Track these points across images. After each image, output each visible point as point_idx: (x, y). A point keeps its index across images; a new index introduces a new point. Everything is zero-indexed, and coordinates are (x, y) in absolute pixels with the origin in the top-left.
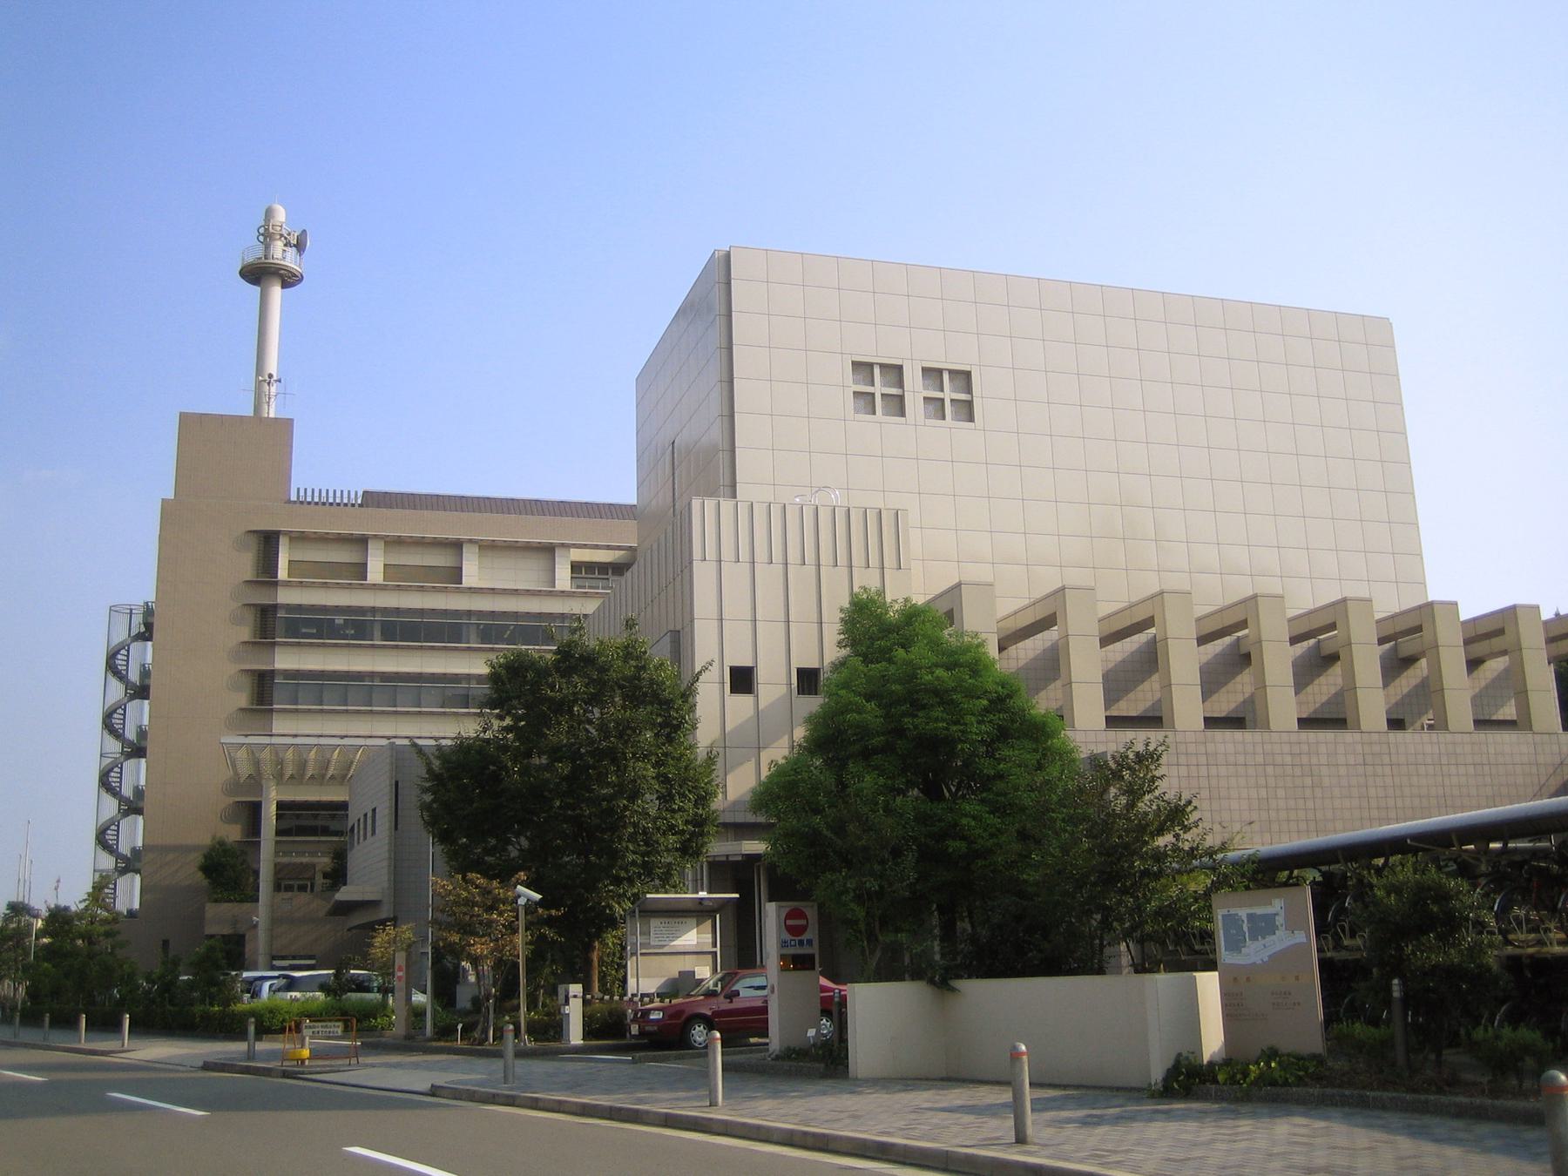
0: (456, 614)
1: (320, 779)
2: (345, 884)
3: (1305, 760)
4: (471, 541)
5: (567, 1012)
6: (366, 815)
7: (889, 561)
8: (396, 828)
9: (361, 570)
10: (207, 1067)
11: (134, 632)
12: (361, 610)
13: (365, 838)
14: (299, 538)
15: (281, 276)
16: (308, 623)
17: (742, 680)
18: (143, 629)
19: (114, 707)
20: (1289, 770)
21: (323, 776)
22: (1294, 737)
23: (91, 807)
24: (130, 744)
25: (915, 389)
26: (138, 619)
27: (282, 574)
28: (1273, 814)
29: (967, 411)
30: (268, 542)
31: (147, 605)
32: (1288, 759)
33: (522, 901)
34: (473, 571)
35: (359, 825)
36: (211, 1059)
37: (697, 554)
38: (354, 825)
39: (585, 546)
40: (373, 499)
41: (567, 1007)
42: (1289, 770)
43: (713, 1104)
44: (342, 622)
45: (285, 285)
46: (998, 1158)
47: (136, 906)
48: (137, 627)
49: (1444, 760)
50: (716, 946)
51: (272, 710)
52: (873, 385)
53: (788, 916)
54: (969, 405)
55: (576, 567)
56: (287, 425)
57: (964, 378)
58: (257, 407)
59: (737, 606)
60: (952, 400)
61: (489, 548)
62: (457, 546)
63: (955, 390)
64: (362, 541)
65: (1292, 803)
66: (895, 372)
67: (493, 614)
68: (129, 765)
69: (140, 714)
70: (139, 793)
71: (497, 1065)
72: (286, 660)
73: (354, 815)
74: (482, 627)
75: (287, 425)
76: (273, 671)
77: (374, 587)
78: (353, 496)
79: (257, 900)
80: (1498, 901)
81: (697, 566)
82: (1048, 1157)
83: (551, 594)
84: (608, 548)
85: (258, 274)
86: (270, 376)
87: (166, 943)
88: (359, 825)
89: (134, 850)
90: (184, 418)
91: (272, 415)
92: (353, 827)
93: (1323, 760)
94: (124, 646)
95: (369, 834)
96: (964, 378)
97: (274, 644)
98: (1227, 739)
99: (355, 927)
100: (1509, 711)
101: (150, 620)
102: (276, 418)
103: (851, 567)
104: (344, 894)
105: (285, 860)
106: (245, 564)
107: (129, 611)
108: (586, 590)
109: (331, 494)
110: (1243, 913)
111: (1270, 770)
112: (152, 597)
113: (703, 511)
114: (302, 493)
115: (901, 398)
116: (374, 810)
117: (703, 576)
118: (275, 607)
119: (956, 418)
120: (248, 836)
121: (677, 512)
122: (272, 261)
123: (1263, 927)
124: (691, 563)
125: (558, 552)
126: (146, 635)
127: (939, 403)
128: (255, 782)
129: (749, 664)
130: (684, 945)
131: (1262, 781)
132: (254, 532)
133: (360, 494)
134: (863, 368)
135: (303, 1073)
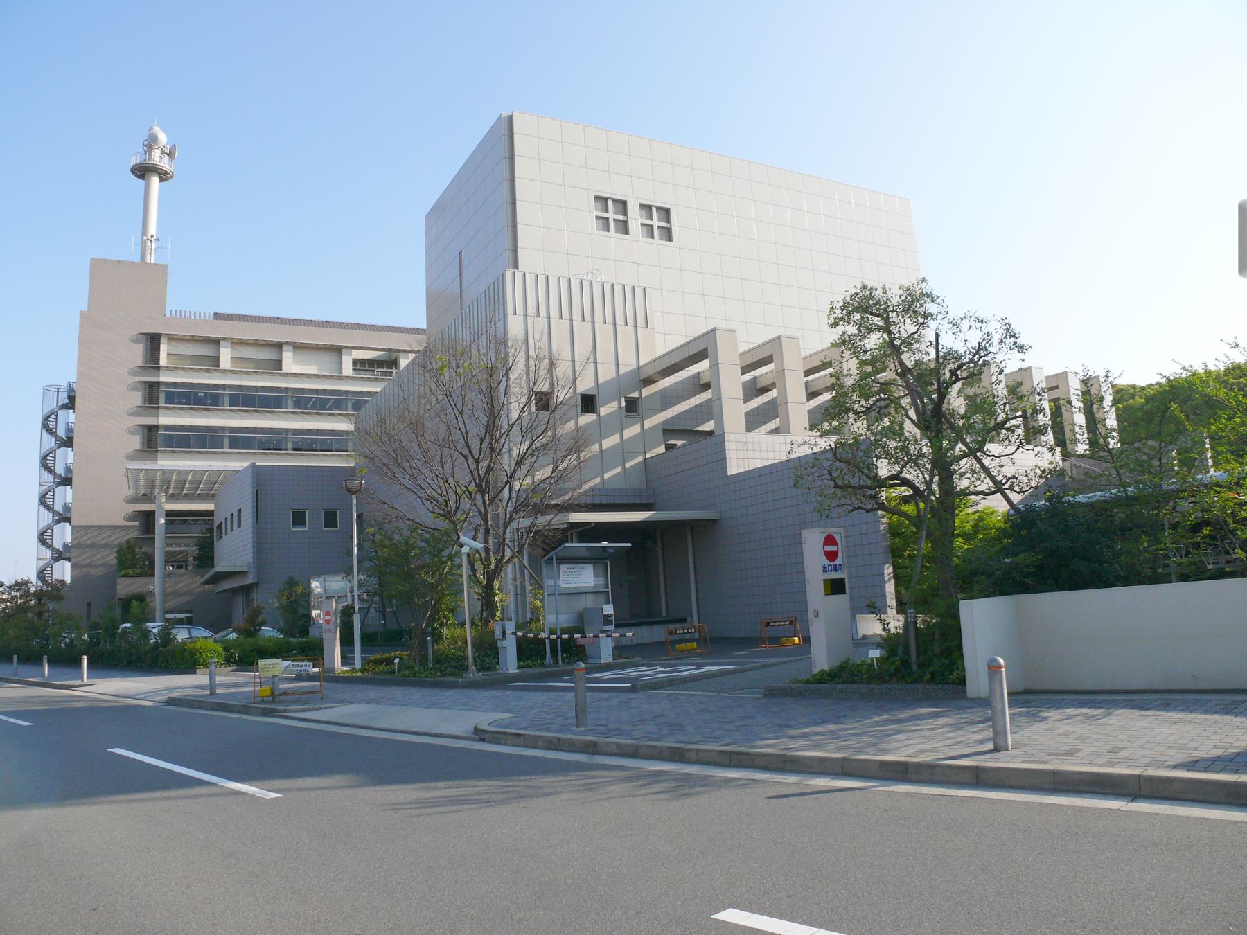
0: (279, 389)
4: (287, 343)
5: (505, 646)
6: (232, 515)
7: (640, 322)
9: (216, 361)
10: (171, 702)
11: (60, 404)
12: (216, 386)
13: (232, 530)
14: (172, 338)
15: (159, 173)
19: (47, 453)
21: (194, 494)
23: (37, 518)
24: (58, 551)
25: (635, 218)
27: (163, 361)
29: (667, 234)
30: (153, 341)
31: (70, 385)
33: (465, 550)
34: (290, 362)
35: (226, 523)
36: (174, 695)
38: (221, 523)
39: (361, 348)
41: (504, 641)
44: (203, 395)
45: (161, 180)
46: (1092, 773)
48: (63, 398)
50: (608, 587)
54: (669, 230)
55: (355, 362)
56: (163, 268)
57: (665, 213)
60: (659, 227)
61: (298, 347)
62: (279, 346)
64: (216, 342)
66: (622, 205)
67: (302, 390)
68: (59, 490)
69: (66, 457)
70: (67, 508)
72: (166, 419)
74: (294, 399)
75: (163, 268)
77: (224, 371)
79: (153, 575)
80: (608, 563)
81: (510, 318)
82: (1100, 766)
83: (340, 378)
84: (376, 349)
85: (142, 171)
87: (89, 604)
88: (226, 523)
89: (65, 545)
90: (95, 262)
91: (153, 262)
94: (54, 412)
95: (229, 531)
99: (224, 591)
101: (72, 394)
106: (138, 353)
107: (56, 390)
108: (362, 376)
112: (73, 378)
116: (239, 511)
118: (156, 427)
120: (143, 534)
121: (466, 306)
122: (153, 162)
125: (344, 351)
128: (148, 497)
130: (585, 587)
132: (145, 334)
133: (212, 315)
134: (602, 200)
135: (285, 711)
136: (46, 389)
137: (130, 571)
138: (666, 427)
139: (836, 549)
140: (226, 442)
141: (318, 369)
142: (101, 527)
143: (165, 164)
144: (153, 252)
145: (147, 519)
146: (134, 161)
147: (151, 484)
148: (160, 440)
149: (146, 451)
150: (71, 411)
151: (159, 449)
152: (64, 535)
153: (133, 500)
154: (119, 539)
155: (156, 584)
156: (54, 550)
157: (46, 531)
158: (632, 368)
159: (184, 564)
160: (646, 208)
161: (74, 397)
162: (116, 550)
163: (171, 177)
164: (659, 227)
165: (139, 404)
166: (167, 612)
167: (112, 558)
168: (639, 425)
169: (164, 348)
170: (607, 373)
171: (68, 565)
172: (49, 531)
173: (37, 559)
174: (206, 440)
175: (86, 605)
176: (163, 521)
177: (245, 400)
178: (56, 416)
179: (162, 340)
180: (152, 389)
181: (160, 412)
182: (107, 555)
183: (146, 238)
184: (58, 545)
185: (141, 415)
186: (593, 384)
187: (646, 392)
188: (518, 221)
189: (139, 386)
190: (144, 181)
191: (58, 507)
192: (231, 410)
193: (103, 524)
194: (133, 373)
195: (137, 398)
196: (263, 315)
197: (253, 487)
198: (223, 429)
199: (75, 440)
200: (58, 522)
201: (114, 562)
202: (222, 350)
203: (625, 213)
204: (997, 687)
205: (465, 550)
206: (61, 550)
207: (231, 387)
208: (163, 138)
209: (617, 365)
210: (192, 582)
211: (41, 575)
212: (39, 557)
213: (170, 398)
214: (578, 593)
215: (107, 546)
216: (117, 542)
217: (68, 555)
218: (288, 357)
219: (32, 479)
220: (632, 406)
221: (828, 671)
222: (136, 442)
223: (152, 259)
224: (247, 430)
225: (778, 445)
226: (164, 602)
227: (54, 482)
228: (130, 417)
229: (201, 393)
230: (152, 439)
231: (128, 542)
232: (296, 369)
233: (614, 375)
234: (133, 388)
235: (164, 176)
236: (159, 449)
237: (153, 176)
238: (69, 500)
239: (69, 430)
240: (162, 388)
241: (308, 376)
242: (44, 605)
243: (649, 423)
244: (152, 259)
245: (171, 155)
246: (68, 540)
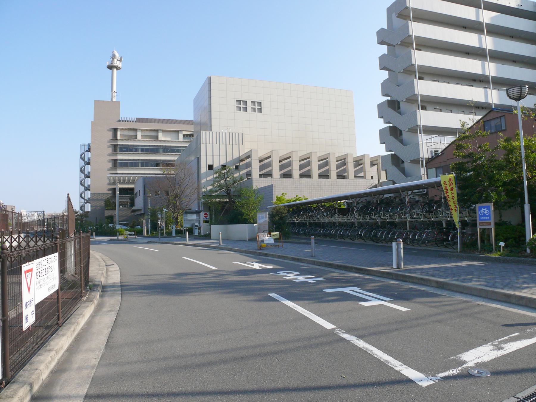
1: (128, 183)
2: (134, 206)
3: (319, 184)
6: (138, 192)
8: (144, 195)
9: (136, 137)
11: (86, 150)
15: (116, 68)
16: (124, 148)
17: (211, 167)
18: (88, 149)
20: (316, 186)
22: (317, 180)
24: (86, 175)
25: (250, 106)
26: (87, 147)
27: (119, 138)
28: (312, 195)
29: (260, 110)
30: (115, 130)
32: (316, 184)
33: (164, 211)
34: (161, 137)
37: (202, 142)
39: (186, 131)
40: (139, 120)
42: (316, 186)
43: (187, 242)
45: (117, 70)
47: (89, 210)
48: (87, 149)
49: (348, 185)
51: (117, 153)
52: (241, 105)
53: (204, 214)
55: (184, 135)
56: (119, 102)
57: (260, 104)
58: (112, 99)
59: (209, 152)
60: (257, 108)
61: (164, 131)
63: (258, 106)
64: (136, 130)
65: (316, 193)
67: (165, 146)
68: (86, 179)
69: (88, 168)
70: (89, 186)
71: (158, 239)
72: (120, 157)
73: (136, 191)
75: (119, 102)
76: (117, 159)
77: (139, 140)
78: (134, 119)
79: (116, 209)
81: (202, 145)
85: (111, 67)
86: (114, 91)
87: (96, 218)
91: (115, 101)
92: (135, 194)
93: (323, 184)
95: (139, 195)
96: (260, 104)
97: (117, 153)
98: (305, 180)
100: (362, 174)
102: (116, 101)
103: (233, 145)
104: (134, 208)
105: (121, 200)
106: (110, 134)
109: (129, 118)
110: (260, 215)
111: (312, 186)
112: (89, 142)
113: (203, 133)
114: (122, 118)
115: (246, 108)
116: (140, 191)
117: (203, 146)
118: (117, 160)
119: (258, 112)
123: (263, 218)
124: (200, 144)
126: (89, 150)
127: (260, 103)
128: (114, 183)
129: (212, 164)
131: (311, 188)
134: (239, 101)
136: (81, 145)
137: (109, 208)
138: (247, 173)
140: (140, 164)
141: (171, 139)
142: (99, 193)
143: (119, 64)
144: (115, 97)
145: (114, 190)
146: (108, 63)
147: (115, 180)
148: (118, 164)
150: (89, 152)
151: (118, 167)
152: (88, 195)
153: (109, 184)
154: (105, 197)
155: (116, 212)
156: (85, 200)
157: (82, 194)
158: (237, 157)
159: (126, 205)
160: (254, 103)
161: (90, 149)
162: (104, 201)
163: (121, 69)
164: (257, 108)
166: (120, 221)
167: (103, 204)
168: (239, 173)
169: (119, 133)
170: (229, 159)
171: (89, 205)
172: (83, 181)
173: (80, 203)
174: (133, 164)
176: (118, 193)
177: (146, 150)
178: (85, 154)
179: (118, 130)
180: (115, 147)
181: (118, 154)
182: (102, 203)
183: (112, 92)
184: (86, 198)
185: (112, 156)
186: (225, 162)
187: (241, 164)
188: (212, 110)
189: (111, 146)
191: (86, 173)
192: (141, 153)
194: (109, 142)
195: (110, 150)
196: (153, 118)
197: (143, 184)
198: (139, 160)
199: (91, 163)
200: (86, 190)
201: (104, 205)
202: (138, 133)
203: (246, 105)
205: (164, 211)
206: (87, 187)
207: (141, 146)
208: (117, 55)
209: (233, 156)
210: (127, 212)
211: (81, 209)
212: (81, 202)
213: (121, 150)
214: (192, 220)
215: (101, 200)
216: (104, 198)
217: (89, 202)
218: (160, 135)
219: (77, 176)
220: (237, 168)
221: (26, 219)
222: (110, 165)
223: (115, 100)
224: (147, 160)
225: (25, 239)
226: (119, 219)
227: (84, 177)
229: (131, 148)
230: (116, 163)
231: (108, 198)
232: (163, 139)
233: (232, 159)
234: (109, 147)
236: (118, 167)
238: (89, 170)
239: (89, 160)
240: (118, 147)
242: (83, 219)
243: (242, 173)
244: (115, 100)
245: (120, 60)
246: (89, 197)
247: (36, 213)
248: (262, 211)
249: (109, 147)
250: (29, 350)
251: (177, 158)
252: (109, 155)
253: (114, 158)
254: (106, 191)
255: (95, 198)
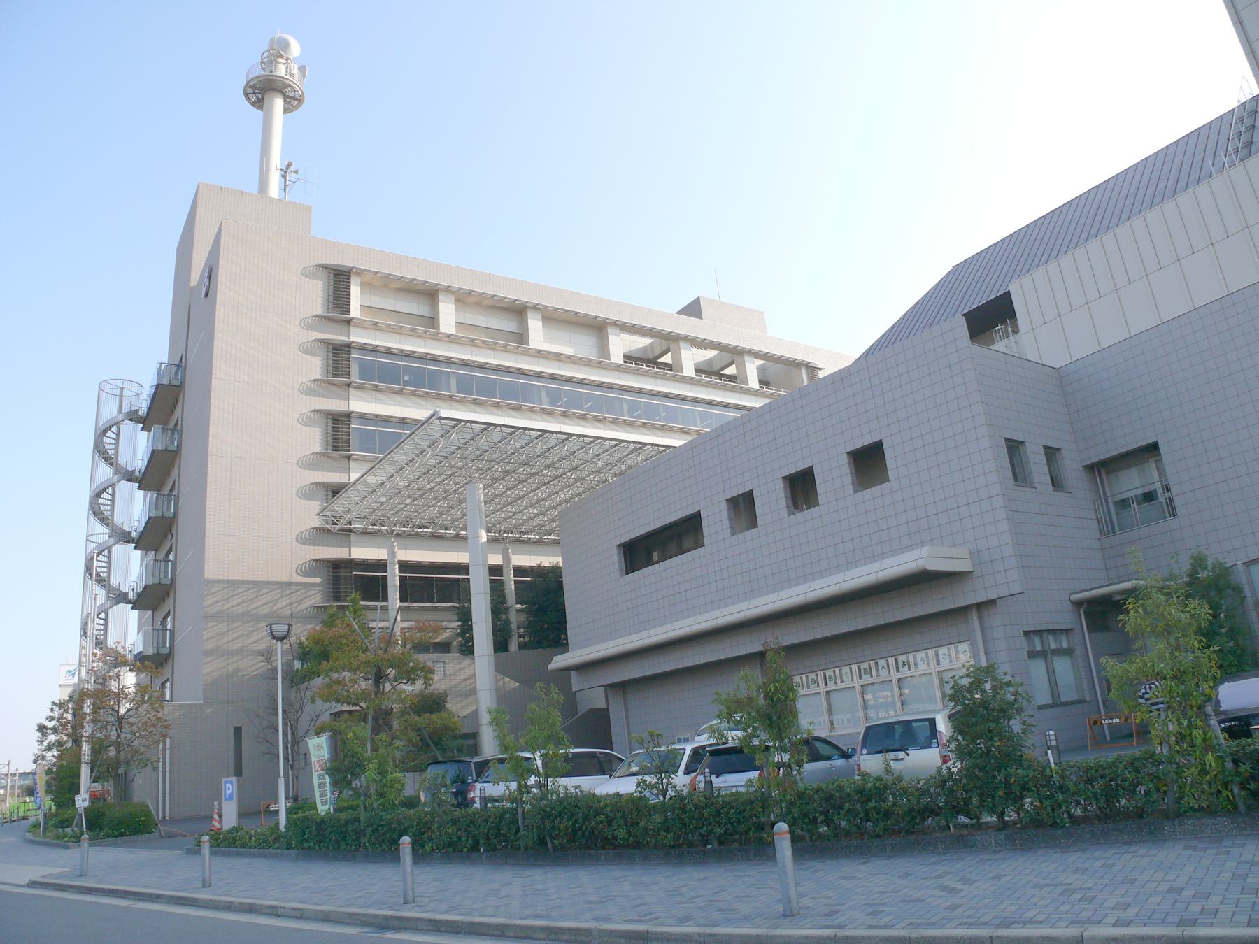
11: (125, 409)
27: (355, 312)
87: (238, 731)
106: (315, 296)
120: (328, 601)
139: (604, 706)
142: (258, 584)
149: (329, 457)
165: (318, 377)
175: (231, 732)
180: (339, 355)
190: (262, 113)
193: (260, 579)
195: (315, 366)
204: (1086, 903)
208: (295, 49)
215: (246, 617)
218: (535, 325)
228: (304, 396)
235: (293, 101)
237: (278, 98)
241: (558, 357)
247: (1045, 801)
248: (802, 869)
249: (306, 494)
250: (227, 842)
251: (684, 442)
252: (306, 465)
253: (337, 405)
254: (287, 573)
255: (240, 610)
